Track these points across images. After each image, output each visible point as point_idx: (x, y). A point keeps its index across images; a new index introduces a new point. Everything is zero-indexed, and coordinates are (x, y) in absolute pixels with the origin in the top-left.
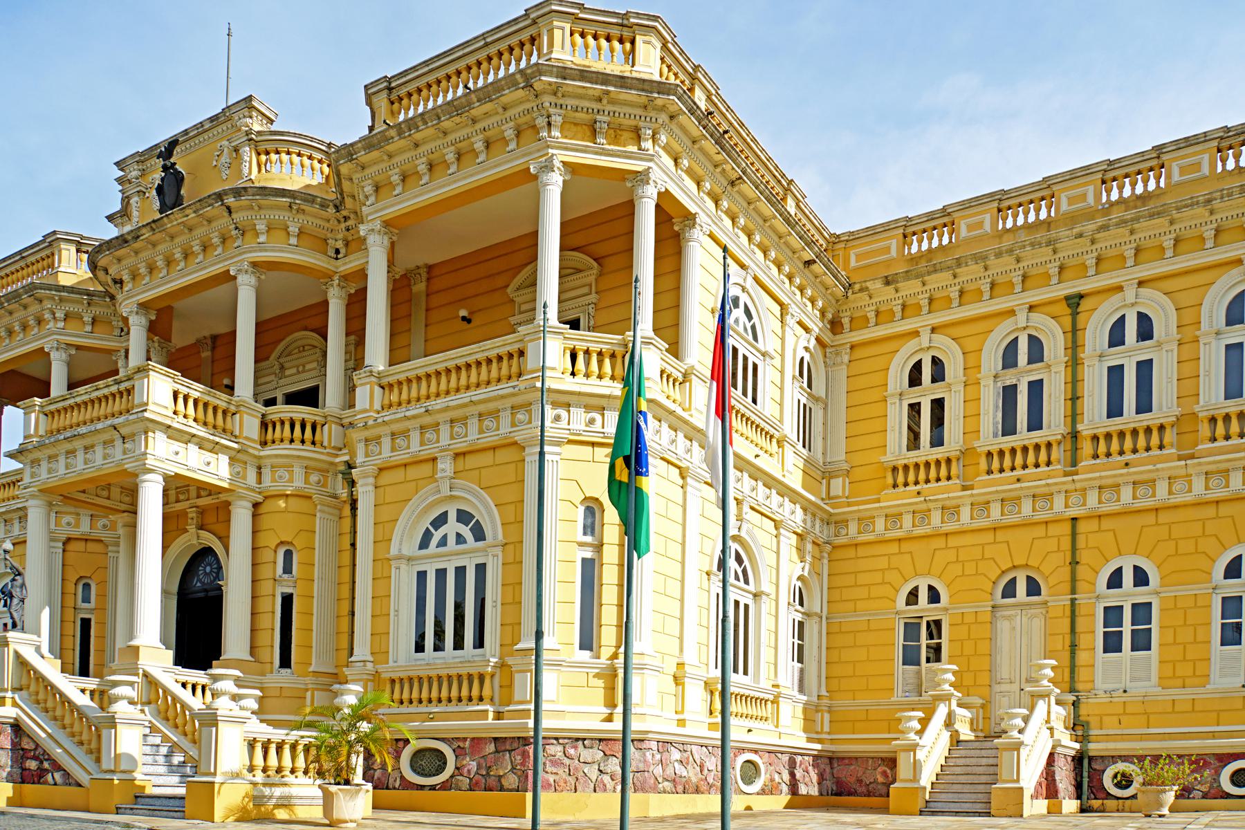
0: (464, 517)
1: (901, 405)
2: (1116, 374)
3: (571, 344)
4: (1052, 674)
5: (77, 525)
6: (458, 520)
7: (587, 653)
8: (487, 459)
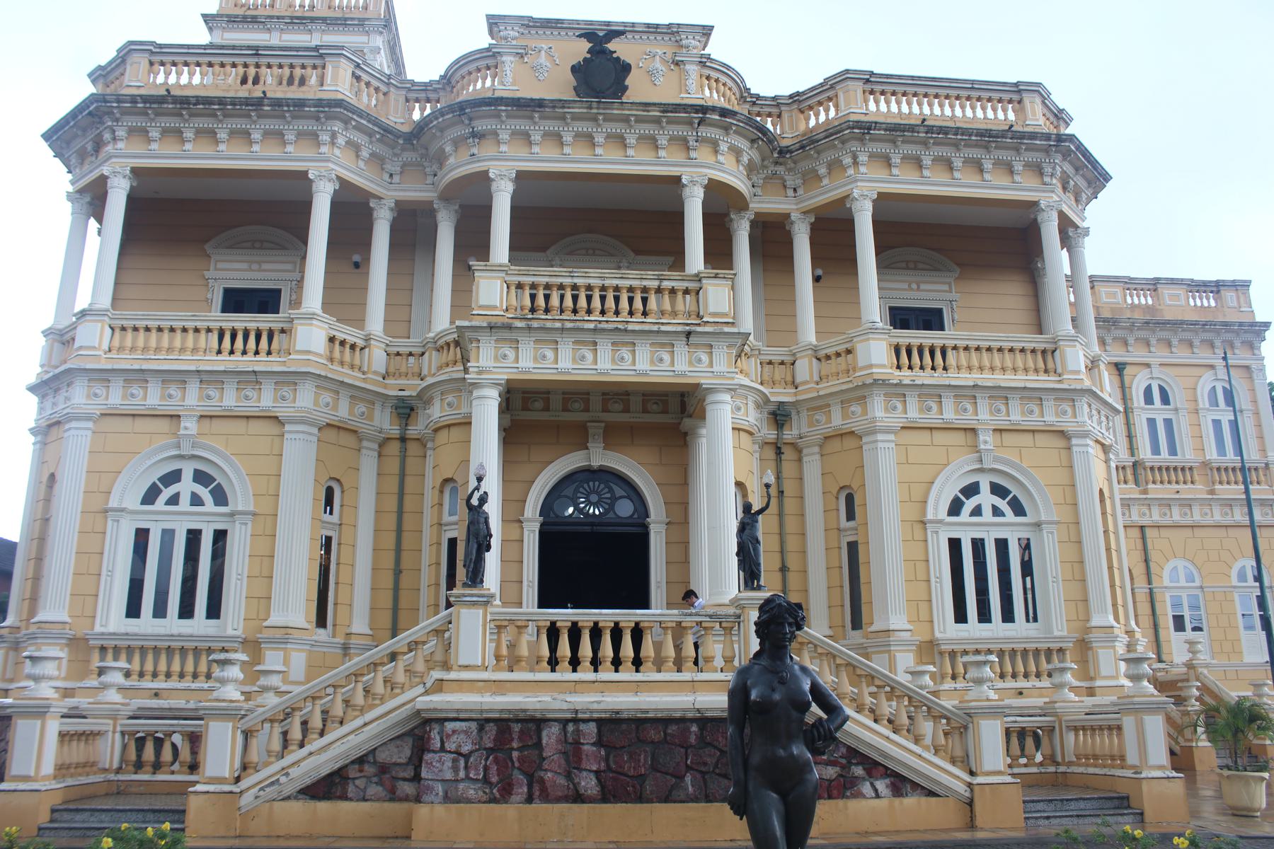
2: (1152, 422)
3: (895, 341)
5: (335, 408)
6: (992, 493)
7: (321, 631)
8: (240, 426)
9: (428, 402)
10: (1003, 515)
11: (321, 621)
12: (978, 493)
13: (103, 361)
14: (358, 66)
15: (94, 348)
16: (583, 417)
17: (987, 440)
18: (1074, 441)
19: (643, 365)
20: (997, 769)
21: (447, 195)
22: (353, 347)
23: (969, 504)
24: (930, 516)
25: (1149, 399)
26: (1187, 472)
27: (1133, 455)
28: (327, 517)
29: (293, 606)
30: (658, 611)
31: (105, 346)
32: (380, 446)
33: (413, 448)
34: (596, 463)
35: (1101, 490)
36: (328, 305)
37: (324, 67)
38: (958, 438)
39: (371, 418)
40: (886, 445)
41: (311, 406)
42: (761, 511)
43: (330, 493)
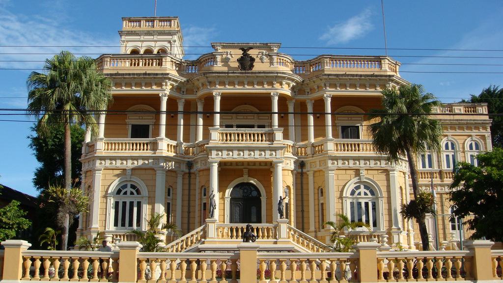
0: (133, 187)
8: (143, 172)
9: (197, 162)
10: (126, 191)
13: (103, 153)
14: (172, 58)
15: (100, 149)
16: (242, 167)
17: (363, 173)
18: (390, 172)
19: (257, 156)
23: (123, 191)
24: (344, 195)
25: (447, 147)
27: (439, 168)
28: (169, 197)
32: (183, 176)
33: (193, 176)
36: (167, 135)
38: (352, 172)
40: (332, 174)
42: (284, 198)
43: (169, 190)
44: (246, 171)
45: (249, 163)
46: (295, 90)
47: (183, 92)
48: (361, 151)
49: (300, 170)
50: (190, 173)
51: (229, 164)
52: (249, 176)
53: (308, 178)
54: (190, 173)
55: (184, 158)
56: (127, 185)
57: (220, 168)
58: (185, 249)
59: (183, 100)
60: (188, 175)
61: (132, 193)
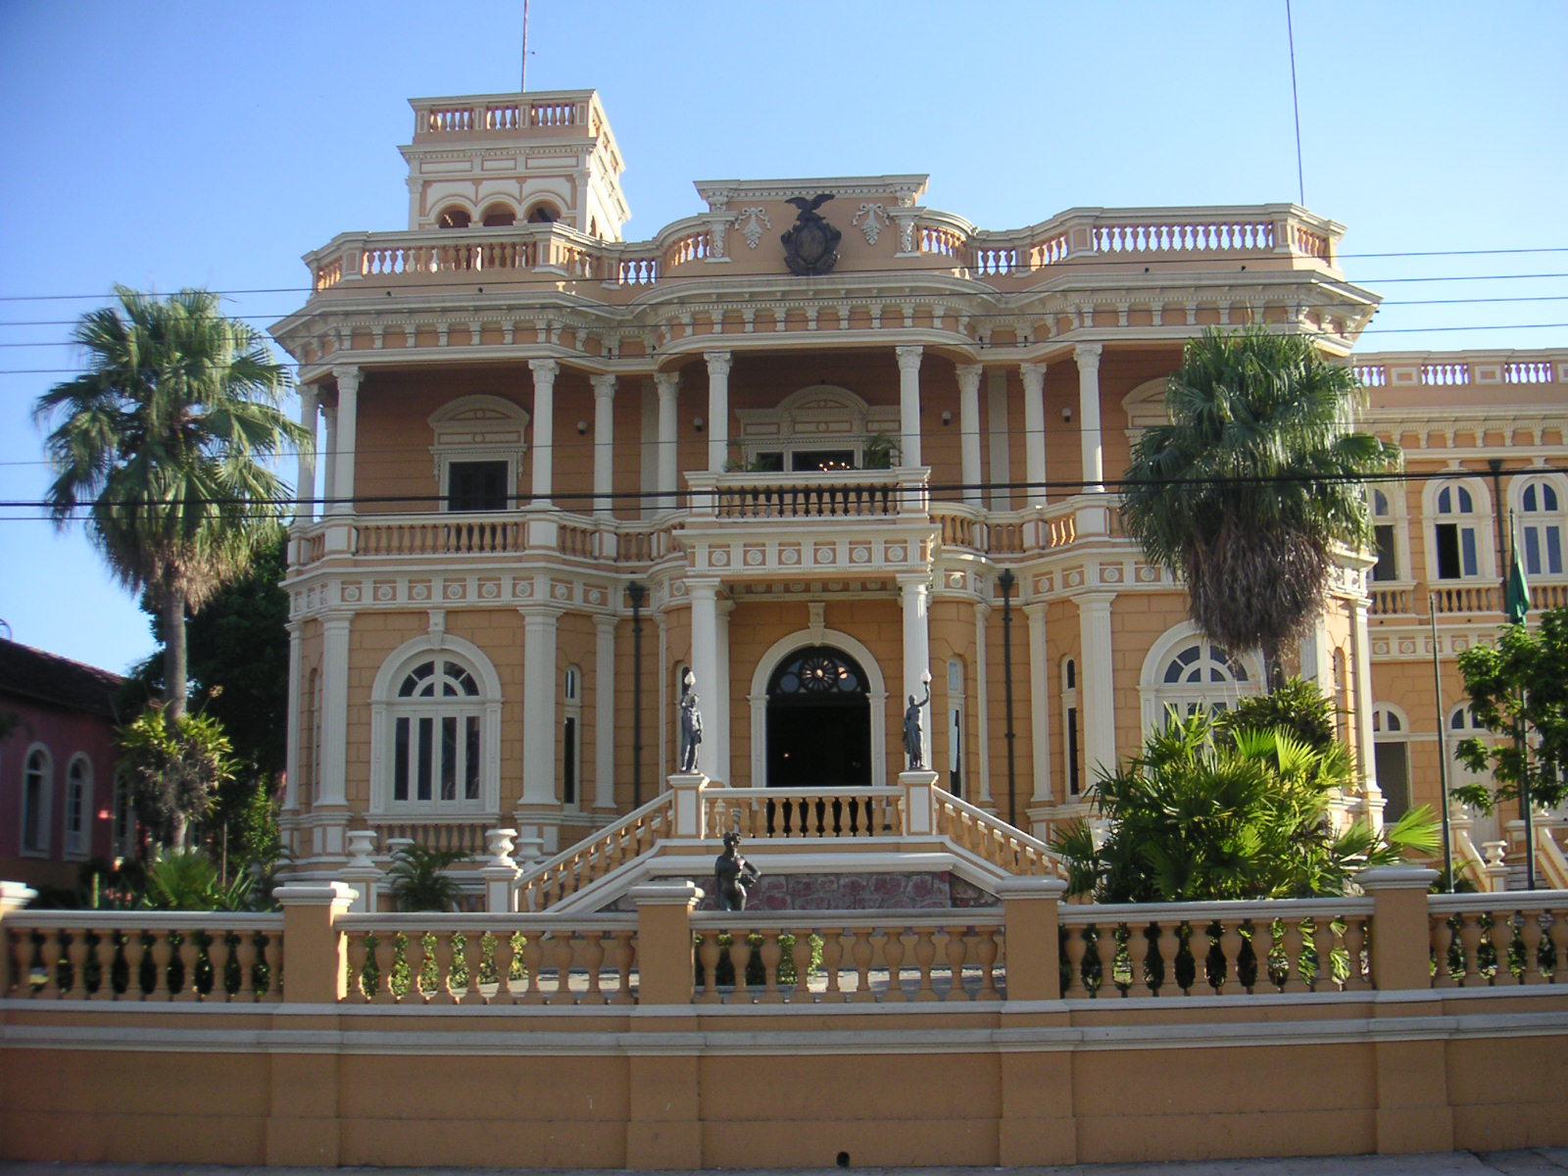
0: (454, 670)
1: (401, 704)
4: (1503, 854)
10: (1198, 671)
11: (569, 798)
12: (1198, 658)
20: (340, 548)
21: (666, 368)
22: (584, 532)
26: (579, 536)
29: (540, 784)
30: (877, 789)
31: (353, 549)
34: (817, 643)
35: (1338, 650)
37: (535, 245)
39: (603, 601)
41: (548, 597)
44: (816, 610)
45: (826, 585)
46: (981, 331)
47: (610, 350)
48: (487, 549)
49: (1000, 602)
50: (637, 620)
51: (798, 587)
52: (825, 627)
53: (1027, 628)
54: (637, 620)
55: (617, 570)
56: (432, 663)
57: (729, 604)
58: (652, 845)
59: (612, 379)
60: (632, 625)
61: (1216, 676)
